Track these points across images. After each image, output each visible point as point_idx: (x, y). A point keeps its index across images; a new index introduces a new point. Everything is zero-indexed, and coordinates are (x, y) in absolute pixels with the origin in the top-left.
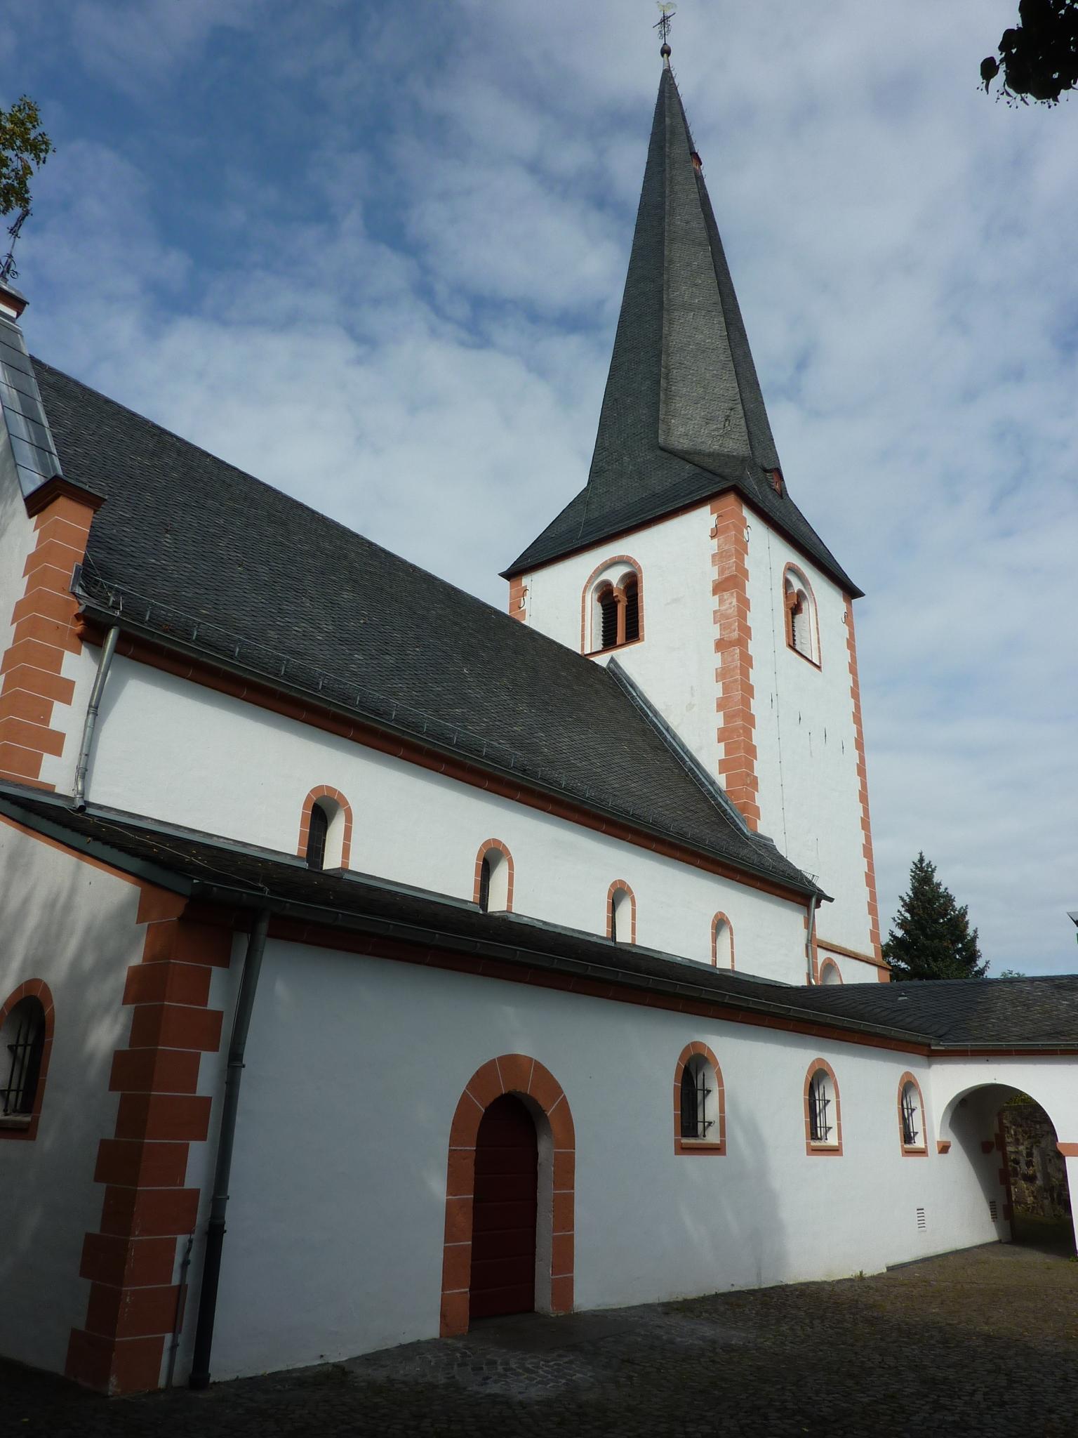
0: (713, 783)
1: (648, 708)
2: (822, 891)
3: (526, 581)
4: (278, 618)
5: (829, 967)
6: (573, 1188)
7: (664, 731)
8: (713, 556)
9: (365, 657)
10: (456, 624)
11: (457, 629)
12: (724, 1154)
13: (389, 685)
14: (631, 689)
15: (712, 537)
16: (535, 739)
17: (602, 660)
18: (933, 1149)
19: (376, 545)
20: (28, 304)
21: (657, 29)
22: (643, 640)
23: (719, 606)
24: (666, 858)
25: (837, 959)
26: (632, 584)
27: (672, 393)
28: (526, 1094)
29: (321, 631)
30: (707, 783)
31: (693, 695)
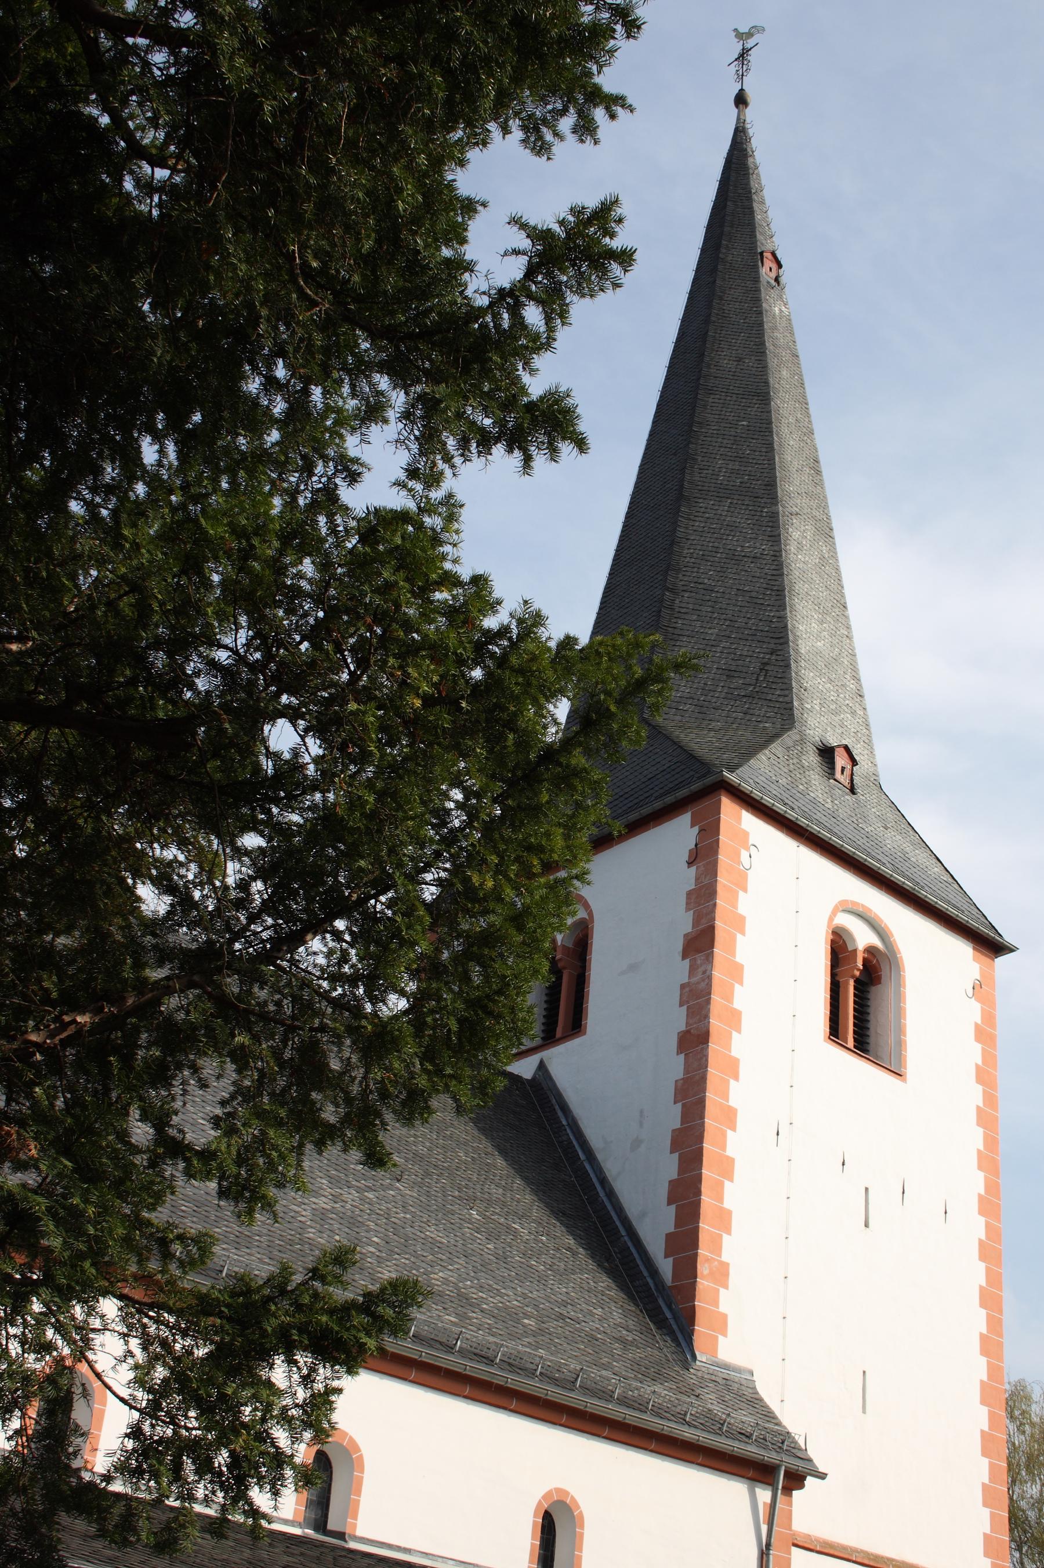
0: (654, 1272)
2: (810, 1460)
8: (689, 894)
14: (560, 1114)
15: (690, 864)
20: (484, 205)
21: (733, 68)
23: (689, 977)
24: (469, 1401)
27: (677, 632)
30: (646, 1273)
31: (641, 1124)
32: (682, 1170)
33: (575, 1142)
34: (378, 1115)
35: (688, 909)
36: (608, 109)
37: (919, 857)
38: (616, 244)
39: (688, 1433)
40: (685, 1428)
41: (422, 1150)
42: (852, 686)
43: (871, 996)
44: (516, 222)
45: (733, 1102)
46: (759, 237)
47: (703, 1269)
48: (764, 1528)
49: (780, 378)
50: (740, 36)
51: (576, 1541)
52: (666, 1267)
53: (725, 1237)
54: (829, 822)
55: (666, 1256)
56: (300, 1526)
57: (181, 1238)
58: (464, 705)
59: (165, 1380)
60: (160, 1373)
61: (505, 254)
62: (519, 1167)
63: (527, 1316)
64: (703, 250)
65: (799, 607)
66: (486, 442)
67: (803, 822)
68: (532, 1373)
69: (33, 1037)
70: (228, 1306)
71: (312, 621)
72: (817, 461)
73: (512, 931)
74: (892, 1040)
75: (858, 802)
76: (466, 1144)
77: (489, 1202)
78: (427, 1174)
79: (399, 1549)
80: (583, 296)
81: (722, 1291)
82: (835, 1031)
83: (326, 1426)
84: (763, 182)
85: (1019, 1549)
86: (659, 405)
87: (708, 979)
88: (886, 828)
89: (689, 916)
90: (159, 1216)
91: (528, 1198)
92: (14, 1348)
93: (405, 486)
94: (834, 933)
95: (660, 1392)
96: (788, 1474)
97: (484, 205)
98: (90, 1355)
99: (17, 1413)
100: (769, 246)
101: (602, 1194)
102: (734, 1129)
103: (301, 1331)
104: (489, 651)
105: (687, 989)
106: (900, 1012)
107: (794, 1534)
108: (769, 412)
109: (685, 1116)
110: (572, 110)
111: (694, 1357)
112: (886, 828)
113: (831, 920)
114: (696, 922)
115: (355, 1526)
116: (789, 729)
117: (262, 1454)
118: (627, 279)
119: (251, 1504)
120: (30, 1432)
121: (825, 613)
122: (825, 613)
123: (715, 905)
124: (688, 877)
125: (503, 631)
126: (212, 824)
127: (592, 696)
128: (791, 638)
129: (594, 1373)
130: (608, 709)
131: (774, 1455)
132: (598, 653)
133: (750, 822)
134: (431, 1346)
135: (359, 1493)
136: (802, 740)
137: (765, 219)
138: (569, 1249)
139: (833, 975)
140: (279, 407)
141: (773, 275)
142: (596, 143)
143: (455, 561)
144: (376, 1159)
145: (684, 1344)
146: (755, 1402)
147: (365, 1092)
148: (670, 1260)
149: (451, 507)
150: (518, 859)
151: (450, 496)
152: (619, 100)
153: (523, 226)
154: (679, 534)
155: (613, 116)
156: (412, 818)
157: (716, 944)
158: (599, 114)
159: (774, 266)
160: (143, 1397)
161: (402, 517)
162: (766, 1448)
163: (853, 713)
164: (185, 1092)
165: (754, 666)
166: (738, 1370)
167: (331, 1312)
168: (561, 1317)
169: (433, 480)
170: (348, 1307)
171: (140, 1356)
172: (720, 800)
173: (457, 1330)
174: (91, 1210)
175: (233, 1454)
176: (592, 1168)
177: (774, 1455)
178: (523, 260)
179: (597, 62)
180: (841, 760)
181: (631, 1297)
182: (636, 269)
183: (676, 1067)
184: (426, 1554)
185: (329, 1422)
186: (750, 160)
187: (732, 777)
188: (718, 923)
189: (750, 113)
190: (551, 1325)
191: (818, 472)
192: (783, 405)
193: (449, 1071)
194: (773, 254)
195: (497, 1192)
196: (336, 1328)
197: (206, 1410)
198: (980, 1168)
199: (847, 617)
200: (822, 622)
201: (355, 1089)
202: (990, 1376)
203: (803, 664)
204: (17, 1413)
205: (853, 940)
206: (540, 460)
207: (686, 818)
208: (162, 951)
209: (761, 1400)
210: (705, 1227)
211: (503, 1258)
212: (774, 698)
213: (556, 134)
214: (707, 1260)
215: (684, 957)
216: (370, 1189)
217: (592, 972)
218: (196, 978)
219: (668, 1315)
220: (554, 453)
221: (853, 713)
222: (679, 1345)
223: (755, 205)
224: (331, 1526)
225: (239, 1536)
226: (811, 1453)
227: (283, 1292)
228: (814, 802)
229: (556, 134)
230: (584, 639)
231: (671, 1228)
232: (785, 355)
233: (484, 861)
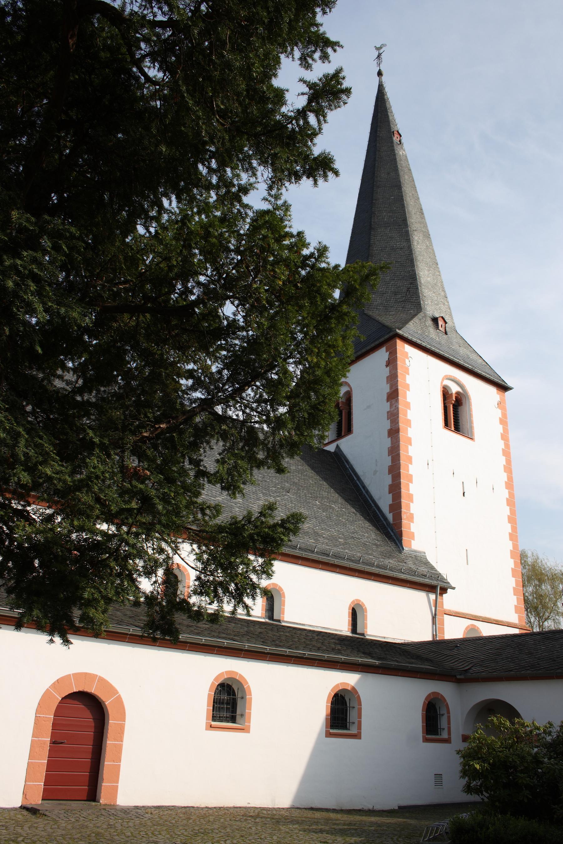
0: (386, 519)
2: (449, 583)
6: (122, 741)
8: (387, 377)
12: (248, 731)
14: (346, 464)
15: (387, 366)
20: (287, 91)
30: (382, 519)
31: (376, 465)
32: (393, 480)
34: (279, 453)
35: (387, 383)
36: (332, 48)
37: (473, 356)
38: (344, 86)
39: (403, 576)
40: (402, 574)
41: (296, 481)
42: (443, 294)
43: (459, 410)
44: (301, 81)
45: (410, 454)
46: (392, 126)
47: (404, 516)
48: (433, 609)
49: (405, 179)
50: (378, 49)
51: (365, 618)
52: (390, 517)
53: (411, 504)
54: (438, 346)
56: (264, 618)
57: (209, 507)
58: (299, 285)
59: (208, 559)
60: (205, 556)
61: (299, 95)
62: (332, 485)
63: (340, 538)
64: (371, 133)
65: (420, 266)
66: (298, 178)
67: (428, 347)
68: (343, 559)
69: (145, 434)
70: (228, 529)
71: (236, 261)
72: (422, 209)
73: (326, 377)
75: (448, 338)
76: (312, 477)
77: (323, 498)
78: (299, 489)
79: (300, 624)
80: (332, 110)
81: (411, 524)
82: (447, 424)
83: (271, 572)
84: (391, 104)
85: (527, 610)
86: (359, 194)
87: (397, 409)
88: (460, 346)
90: (200, 500)
92: (150, 551)
93: (267, 200)
94: (443, 388)
95: (391, 562)
96: (441, 588)
97: (287, 91)
98: (178, 552)
99: (154, 575)
100: (396, 129)
102: (411, 464)
103: (258, 536)
104: (307, 263)
106: (471, 416)
107: (444, 610)
108: (402, 192)
110: (318, 50)
111: (403, 549)
112: (460, 346)
113: (442, 383)
114: (391, 387)
115: (284, 617)
116: (420, 312)
117: (247, 584)
118: (349, 101)
119: (245, 603)
120: (159, 582)
121: (430, 267)
122: (430, 267)
123: (398, 381)
124: (386, 371)
125: (312, 255)
126: (205, 348)
127: (349, 283)
128: (418, 277)
129: (367, 557)
130: (355, 288)
131: (435, 582)
132: (348, 271)
133: (408, 348)
134: (306, 551)
135: (284, 605)
136: (425, 316)
137: (393, 119)
138: (353, 513)
139: (444, 404)
140: (214, 180)
141: (398, 139)
142: (329, 62)
143: (290, 227)
144: (280, 470)
145: (399, 544)
146: (427, 563)
147: (274, 446)
149: (286, 207)
150: (325, 351)
151: (285, 202)
152: (337, 44)
153: (305, 82)
154: (371, 242)
155: (335, 51)
156: (282, 335)
158: (329, 50)
159: (398, 136)
160: (200, 565)
161: (268, 212)
162: (432, 580)
163: (444, 304)
164: (205, 452)
165: (404, 290)
166: (420, 552)
167: (269, 528)
168: (353, 538)
169: (277, 197)
170: (275, 526)
171: (197, 551)
172: (396, 342)
173: (314, 545)
174: (172, 494)
175: (236, 585)
177: (435, 582)
178: (306, 97)
179: (329, 7)
180: (441, 322)
181: (378, 529)
182: (352, 96)
183: (388, 442)
184: (310, 626)
185: (272, 571)
186: (386, 96)
187: (400, 332)
188: (399, 387)
189: (384, 78)
190: (350, 541)
191: (423, 214)
192: (407, 189)
193: (306, 434)
194: (398, 132)
195: (325, 494)
196: (271, 533)
197: (224, 570)
198: (505, 471)
199: (438, 268)
200: (429, 271)
201: (270, 445)
202: (514, 548)
203: (423, 287)
204: (154, 575)
205: (451, 390)
206: (321, 181)
207: (383, 349)
208: (191, 400)
209: (429, 562)
210: (404, 501)
211: (329, 518)
212: (413, 301)
213: (313, 60)
214: (405, 513)
215: (387, 402)
216: (278, 496)
218: (205, 407)
219: (392, 534)
220: (325, 176)
221: (444, 304)
223: (389, 114)
224: (275, 618)
225: (242, 623)
226: (449, 580)
227: (250, 522)
228: (432, 339)
229: (313, 60)
230: (343, 265)
231: (391, 502)
232: (406, 170)
233: (312, 351)
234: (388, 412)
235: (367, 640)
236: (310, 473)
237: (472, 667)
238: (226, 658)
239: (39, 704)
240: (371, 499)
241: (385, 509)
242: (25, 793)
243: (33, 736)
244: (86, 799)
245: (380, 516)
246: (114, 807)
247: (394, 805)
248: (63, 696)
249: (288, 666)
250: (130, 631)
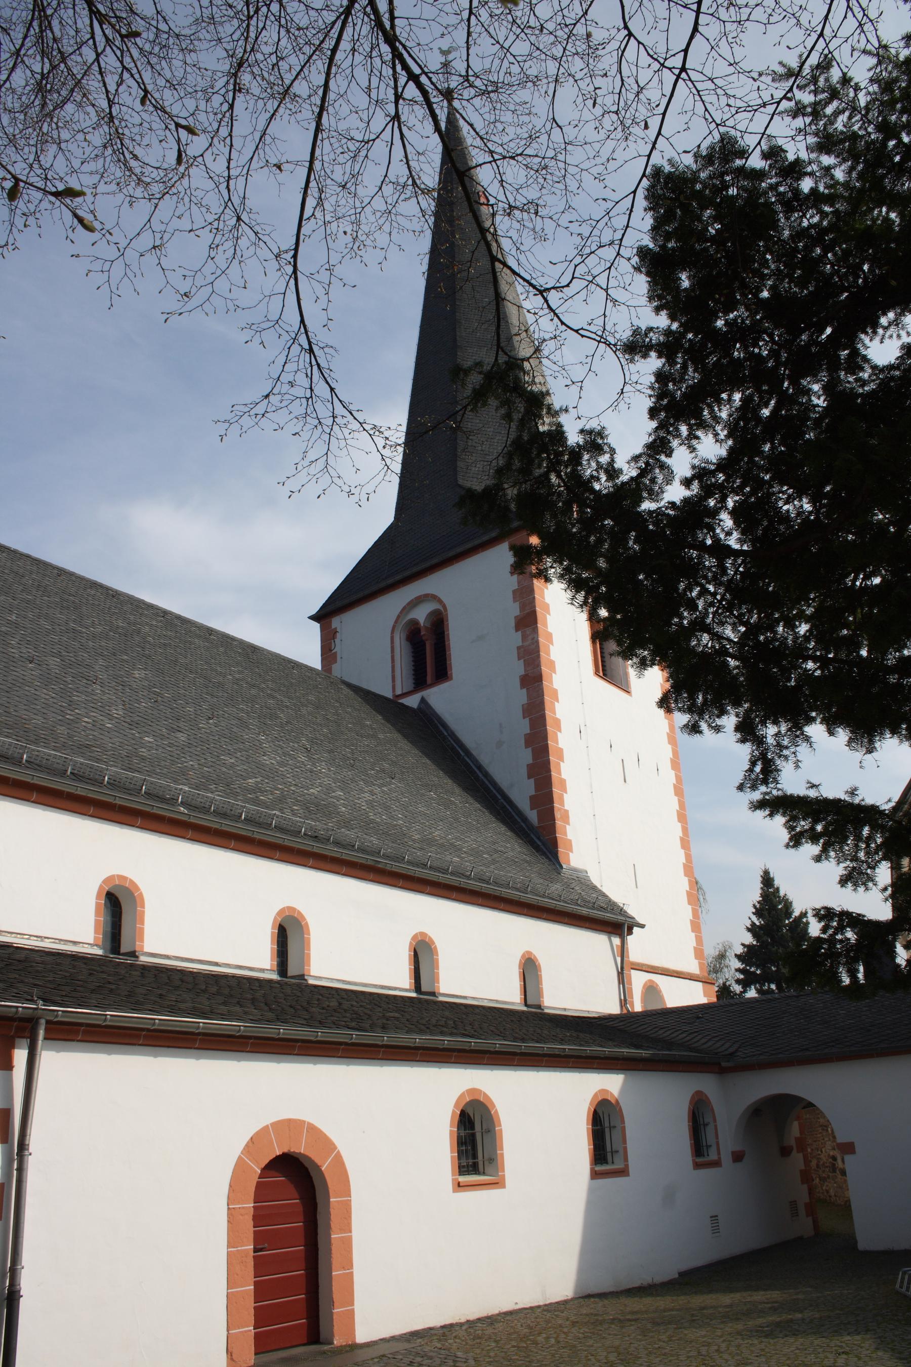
1: (460, 747)
2: (634, 918)
3: (336, 622)
4: (69, 712)
5: (651, 990)
6: (350, 1232)
7: (476, 770)
8: (514, 592)
9: (155, 738)
10: (253, 686)
11: (254, 692)
12: (504, 1186)
13: (179, 765)
14: (441, 728)
16: (332, 800)
17: (412, 701)
18: (726, 1158)
19: (171, 613)
22: (451, 679)
25: (658, 979)
26: (439, 623)
28: (300, 1153)
29: (110, 717)
30: (519, 820)
33: (457, 747)
35: (515, 601)
39: (584, 911)
48: (619, 959)
52: (533, 816)
55: (532, 809)
74: (621, 672)
89: (517, 605)
91: (450, 782)
95: (556, 888)
101: (480, 775)
105: (522, 649)
109: (533, 725)
111: (561, 867)
114: (522, 608)
135: (438, 968)
138: (480, 810)
148: (535, 811)
157: (538, 622)
176: (470, 759)
183: (521, 697)
188: (537, 609)
214: (559, 809)
217: (451, 642)
219: (539, 843)
222: (550, 860)
231: (532, 792)
234: (519, 648)
235: (548, 1014)
236: (404, 745)
237: (739, 1048)
238: (279, 1062)
239: (230, 1186)
240: (495, 788)
241: (523, 804)
242: (230, 1350)
243: (229, 1245)
244: (306, 1342)
245: (514, 814)
246: (354, 1347)
247: (668, 1271)
248: (263, 1166)
249: (315, 1064)
250: (352, 1038)
